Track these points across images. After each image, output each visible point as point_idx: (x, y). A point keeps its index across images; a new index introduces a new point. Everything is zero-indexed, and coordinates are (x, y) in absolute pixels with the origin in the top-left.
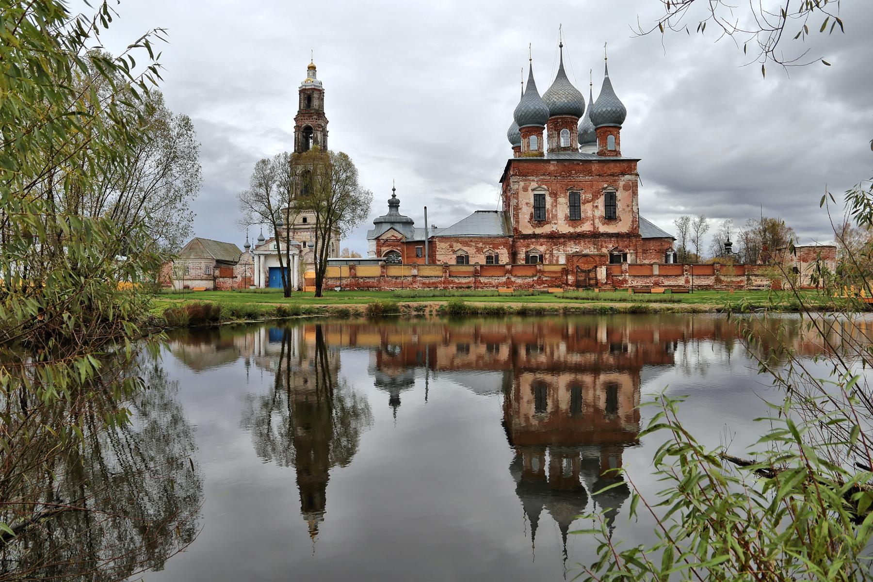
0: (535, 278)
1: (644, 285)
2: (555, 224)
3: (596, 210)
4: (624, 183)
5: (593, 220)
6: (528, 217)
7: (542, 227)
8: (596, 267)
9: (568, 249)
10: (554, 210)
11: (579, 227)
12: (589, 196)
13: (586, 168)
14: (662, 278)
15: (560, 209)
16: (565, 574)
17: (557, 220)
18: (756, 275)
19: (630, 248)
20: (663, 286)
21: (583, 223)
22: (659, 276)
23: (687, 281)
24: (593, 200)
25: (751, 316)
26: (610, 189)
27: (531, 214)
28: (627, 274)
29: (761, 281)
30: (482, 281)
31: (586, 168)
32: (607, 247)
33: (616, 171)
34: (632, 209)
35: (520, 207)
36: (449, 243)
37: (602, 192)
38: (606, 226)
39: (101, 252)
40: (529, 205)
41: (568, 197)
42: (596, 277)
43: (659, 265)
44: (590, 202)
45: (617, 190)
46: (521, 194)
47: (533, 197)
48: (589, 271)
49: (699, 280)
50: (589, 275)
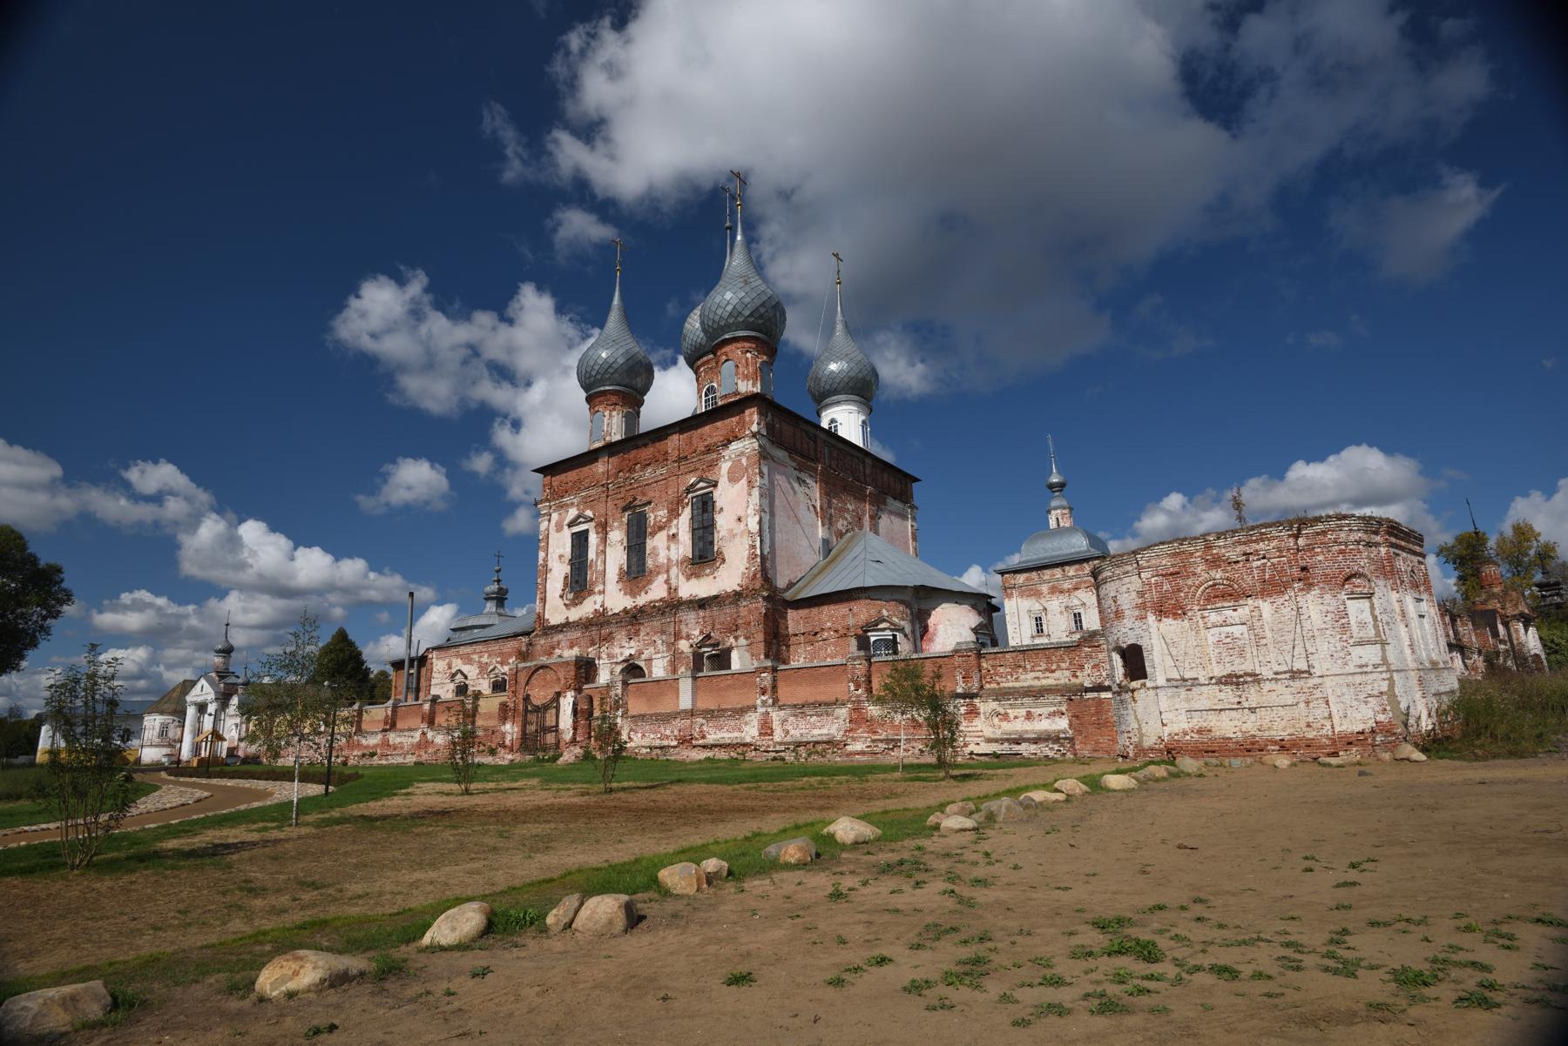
3: (673, 547)
6: (559, 585)
7: (581, 603)
9: (617, 650)
12: (662, 513)
14: (700, 720)
15: (612, 557)
16: (1307, 1021)
18: (1002, 695)
20: (704, 747)
21: (650, 582)
22: (692, 713)
23: (766, 729)
25: (446, 1036)
29: (1029, 716)
30: (391, 743)
32: (688, 637)
33: (715, 440)
35: (549, 567)
37: (686, 497)
38: (694, 581)
39: (498, 686)
41: (625, 527)
42: (557, 726)
45: (715, 486)
46: (553, 535)
47: (570, 540)
48: (546, 707)
49: (802, 723)
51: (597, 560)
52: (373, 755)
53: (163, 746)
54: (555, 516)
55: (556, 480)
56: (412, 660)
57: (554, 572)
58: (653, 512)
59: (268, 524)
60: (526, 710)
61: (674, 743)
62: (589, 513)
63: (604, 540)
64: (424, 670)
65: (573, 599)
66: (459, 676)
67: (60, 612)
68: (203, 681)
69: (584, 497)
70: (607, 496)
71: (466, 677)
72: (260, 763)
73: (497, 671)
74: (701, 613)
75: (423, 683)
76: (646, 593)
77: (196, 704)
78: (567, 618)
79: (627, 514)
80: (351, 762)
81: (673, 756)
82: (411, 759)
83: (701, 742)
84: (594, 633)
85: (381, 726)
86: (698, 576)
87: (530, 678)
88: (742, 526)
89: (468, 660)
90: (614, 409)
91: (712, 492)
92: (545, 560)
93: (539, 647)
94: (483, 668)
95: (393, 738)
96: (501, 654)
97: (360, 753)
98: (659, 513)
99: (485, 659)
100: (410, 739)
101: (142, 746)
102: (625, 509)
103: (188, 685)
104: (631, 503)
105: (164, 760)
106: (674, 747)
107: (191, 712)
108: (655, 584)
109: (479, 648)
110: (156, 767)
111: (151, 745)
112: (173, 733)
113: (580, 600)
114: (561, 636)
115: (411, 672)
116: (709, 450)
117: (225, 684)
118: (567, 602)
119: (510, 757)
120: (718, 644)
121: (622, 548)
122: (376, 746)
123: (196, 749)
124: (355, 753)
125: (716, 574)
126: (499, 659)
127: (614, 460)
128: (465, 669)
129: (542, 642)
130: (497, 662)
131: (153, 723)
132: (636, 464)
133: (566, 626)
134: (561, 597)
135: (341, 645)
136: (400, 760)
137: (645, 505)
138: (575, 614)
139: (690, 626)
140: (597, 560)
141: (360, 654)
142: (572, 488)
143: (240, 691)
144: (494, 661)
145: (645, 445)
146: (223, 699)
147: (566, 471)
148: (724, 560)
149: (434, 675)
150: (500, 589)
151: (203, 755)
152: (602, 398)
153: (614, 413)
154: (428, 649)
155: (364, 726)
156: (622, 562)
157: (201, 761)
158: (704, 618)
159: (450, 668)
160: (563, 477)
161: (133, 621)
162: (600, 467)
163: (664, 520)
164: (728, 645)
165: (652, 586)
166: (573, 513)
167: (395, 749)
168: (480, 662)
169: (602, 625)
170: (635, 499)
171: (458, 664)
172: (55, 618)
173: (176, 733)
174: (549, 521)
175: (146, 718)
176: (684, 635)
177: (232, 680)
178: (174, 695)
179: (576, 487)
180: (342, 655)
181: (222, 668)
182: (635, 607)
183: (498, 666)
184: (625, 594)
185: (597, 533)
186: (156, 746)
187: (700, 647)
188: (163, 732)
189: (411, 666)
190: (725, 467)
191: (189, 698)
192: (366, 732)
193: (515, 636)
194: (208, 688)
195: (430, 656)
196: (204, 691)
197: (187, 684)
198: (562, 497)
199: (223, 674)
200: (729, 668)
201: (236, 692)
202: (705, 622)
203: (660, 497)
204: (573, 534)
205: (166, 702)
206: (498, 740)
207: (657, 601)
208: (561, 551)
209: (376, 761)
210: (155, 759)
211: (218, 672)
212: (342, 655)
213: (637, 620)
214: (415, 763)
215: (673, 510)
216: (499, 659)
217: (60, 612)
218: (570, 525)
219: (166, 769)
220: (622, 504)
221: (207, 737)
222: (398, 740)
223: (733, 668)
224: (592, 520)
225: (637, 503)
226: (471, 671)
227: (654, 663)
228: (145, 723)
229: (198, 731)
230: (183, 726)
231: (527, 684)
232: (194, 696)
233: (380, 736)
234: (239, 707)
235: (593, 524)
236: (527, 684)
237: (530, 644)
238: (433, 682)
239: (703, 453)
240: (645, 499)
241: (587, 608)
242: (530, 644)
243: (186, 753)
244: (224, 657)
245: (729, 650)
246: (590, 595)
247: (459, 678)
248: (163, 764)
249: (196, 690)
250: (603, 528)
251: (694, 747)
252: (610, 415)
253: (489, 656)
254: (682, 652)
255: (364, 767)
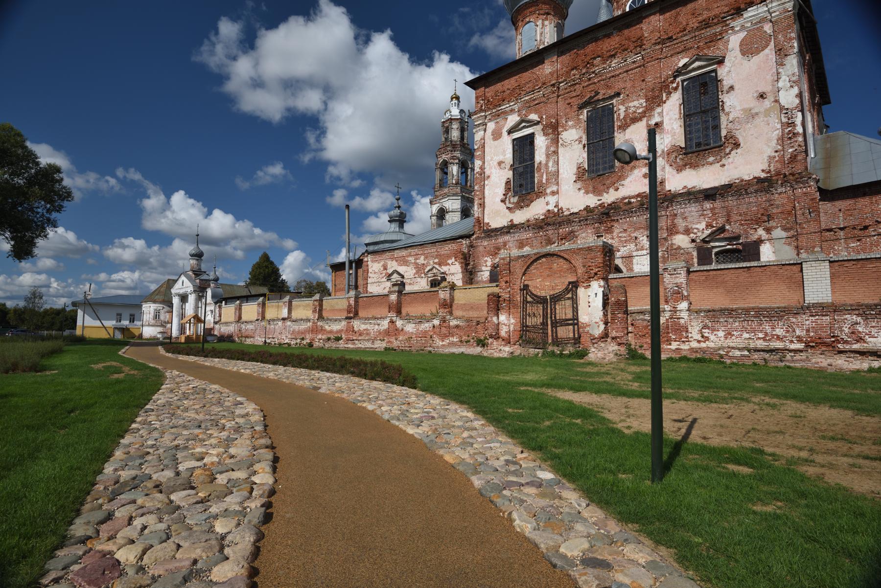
0: (436, 322)
1: (760, 344)
2: (553, 193)
4: (742, 35)
5: (652, 167)
6: (500, 190)
7: (528, 206)
8: (575, 285)
10: (550, 164)
11: (611, 190)
12: (638, 104)
13: (629, 39)
17: (558, 184)
19: (772, 223)
20: (862, 353)
24: (648, 111)
26: (698, 68)
27: (508, 183)
28: (684, 305)
30: (356, 329)
31: (629, 39)
32: (687, 231)
33: (717, 11)
34: (777, 101)
35: (487, 173)
36: (382, 263)
40: (503, 165)
42: (575, 318)
43: (830, 262)
44: (640, 119)
45: (721, 62)
46: (490, 144)
47: (511, 147)
48: (556, 299)
50: (554, 311)
51: (547, 162)
52: (338, 339)
53: (158, 326)
54: (491, 126)
55: (490, 91)
56: (351, 262)
57: (493, 178)
58: (623, 104)
59: (297, 13)
60: (525, 302)
61: (800, 346)
62: (534, 117)
63: (555, 141)
64: (360, 271)
65: (518, 203)
66: (395, 275)
67: (62, 207)
68: (183, 278)
69: (527, 102)
70: (558, 96)
71: (403, 277)
72: (233, 341)
73: (435, 271)
74: (708, 205)
75: (361, 282)
76: (617, 189)
77: (179, 295)
78: (511, 221)
79: (585, 111)
80: (316, 344)
81: (799, 362)
82: (380, 345)
83: (856, 346)
84: (550, 232)
85: (345, 315)
86: (694, 166)
87: (528, 267)
88: (767, 103)
89: (404, 262)
90: (546, 19)
91: (715, 71)
92: (482, 168)
93: (481, 249)
94: (419, 269)
95: (357, 324)
96: (438, 256)
97: (324, 337)
98: (631, 104)
99: (421, 260)
100: (377, 327)
101: (142, 326)
102: (581, 108)
103: (171, 283)
104: (591, 98)
105: (159, 336)
106: (796, 351)
107: (176, 301)
108: (628, 180)
109: (413, 251)
110: (153, 342)
111: (149, 325)
112: (164, 316)
113: (527, 202)
114: (507, 238)
115: (351, 272)
116: (706, 24)
117: (200, 280)
118: (511, 206)
119: (507, 349)
120: (737, 238)
121: (581, 146)
122: (340, 331)
123: (182, 329)
124: (320, 336)
125: (724, 161)
126: (436, 260)
127: (566, 58)
128: (402, 269)
129: (486, 243)
130: (435, 263)
131: (149, 309)
132: (595, 58)
133: (511, 228)
134: (503, 201)
135: (265, 264)
136: (368, 345)
137: (612, 97)
138: (520, 217)
139: (689, 219)
140: (547, 162)
141: (278, 270)
142: (511, 95)
143: (212, 285)
144: (431, 262)
145: (608, 36)
146: (201, 290)
147: (501, 80)
148: (737, 145)
149: (370, 275)
150: (401, 213)
151: (188, 333)
152: (533, 9)
153: (546, 23)
154: (363, 254)
155: (325, 314)
156: (581, 160)
157: (188, 338)
158: (712, 209)
159: (385, 269)
160: (499, 86)
161: (127, 255)
162: (547, 68)
163: (640, 110)
164: (755, 237)
165: (625, 182)
166: (513, 119)
167: (360, 335)
168: (416, 263)
169: (560, 224)
170: (597, 93)
171: (393, 266)
172: (58, 211)
173: (166, 317)
174: (485, 130)
175: (144, 306)
176: (681, 229)
177: (204, 277)
178: (162, 290)
179: (515, 94)
180: (267, 270)
181: (196, 268)
182: (600, 205)
183: (437, 266)
184: (587, 192)
185: (545, 134)
186: (152, 326)
187: (708, 242)
188: (157, 316)
189: (351, 268)
190: (735, 40)
191: (173, 291)
192: (328, 319)
193: (454, 239)
194: (187, 283)
195: (366, 259)
196: (184, 285)
197: (170, 282)
198: (500, 105)
199: (197, 273)
200: (759, 259)
201: (209, 286)
202: (714, 214)
203: (634, 87)
204: (514, 140)
205: (157, 295)
206: (491, 331)
207: (633, 197)
208: (501, 158)
209: (341, 344)
210: (153, 335)
211: (193, 271)
212: (267, 270)
213: (610, 217)
214: (386, 349)
215: (654, 98)
216: (436, 260)
217: (62, 207)
218: (510, 132)
219: (162, 344)
220: (576, 102)
221: (190, 320)
222: (363, 327)
223: (762, 260)
224: (538, 123)
225: (600, 97)
226: (408, 271)
227: (635, 261)
228: (143, 309)
229: (182, 316)
230: (172, 312)
231: (524, 274)
232: (177, 289)
233: (344, 323)
234: (213, 297)
235: (539, 127)
236: (524, 274)
237: (472, 246)
238: (370, 281)
239: (698, 29)
240: (611, 92)
241: (537, 209)
242: (472, 246)
243: (175, 333)
244: (197, 260)
245: (759, 242)
246: (538, 197)
247: (395, 277)
248: (158, 339)
249: (178, 285)
250: (554, 129)
251: (841, 352)
252: (543, 24)
253: (426, 258)
254: (679, 248)
255: (329, 350)
